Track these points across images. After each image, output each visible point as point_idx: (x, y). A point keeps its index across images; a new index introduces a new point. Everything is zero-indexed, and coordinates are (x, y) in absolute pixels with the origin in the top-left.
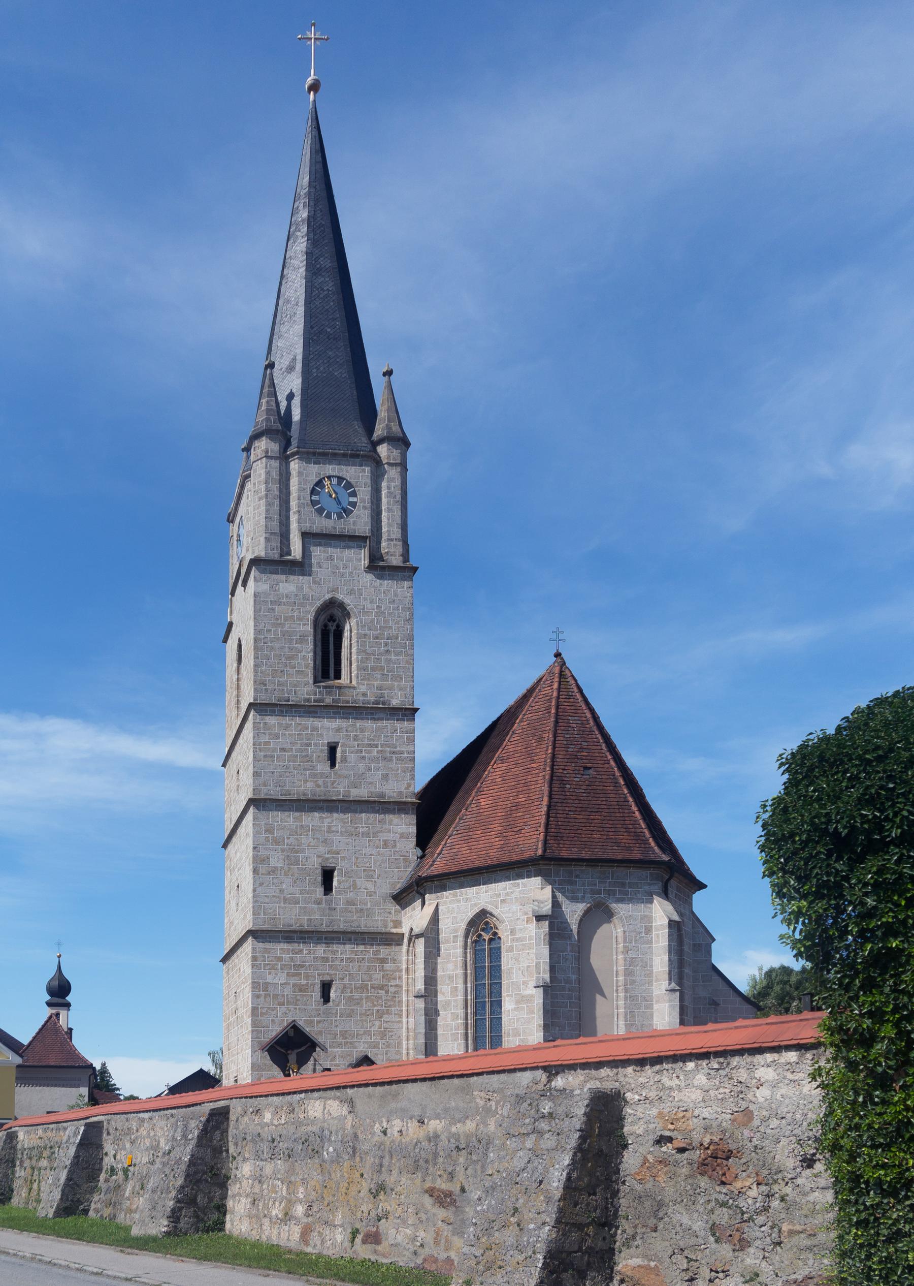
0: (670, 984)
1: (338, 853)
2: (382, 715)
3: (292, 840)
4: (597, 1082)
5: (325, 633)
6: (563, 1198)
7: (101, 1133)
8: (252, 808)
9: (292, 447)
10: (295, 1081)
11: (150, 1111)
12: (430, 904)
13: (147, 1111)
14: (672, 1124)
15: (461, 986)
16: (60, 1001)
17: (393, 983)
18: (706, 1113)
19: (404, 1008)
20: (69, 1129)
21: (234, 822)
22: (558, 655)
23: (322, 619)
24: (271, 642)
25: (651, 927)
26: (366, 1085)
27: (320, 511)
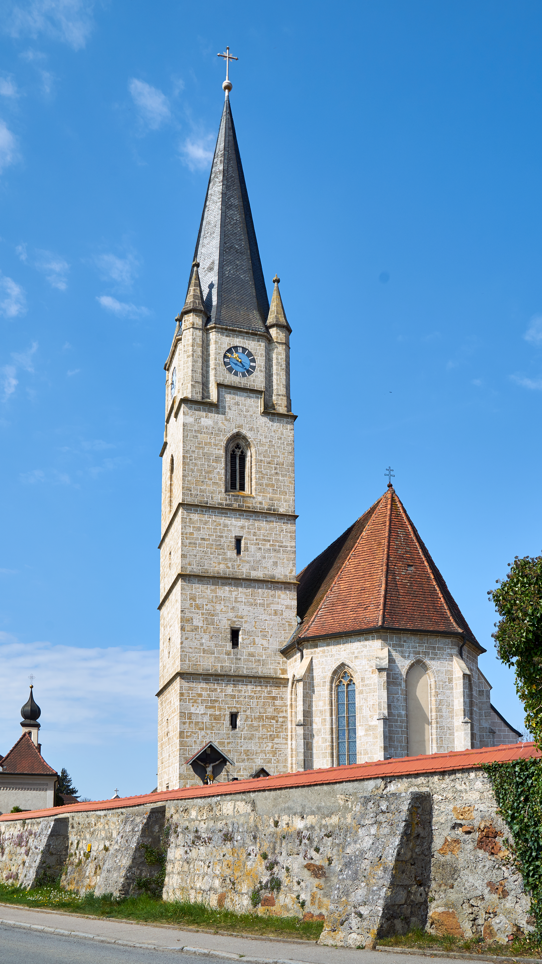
1: (242, 618)
2: (273, 519)
3: (209, 606)
4: (416, 787)
6: (395, 868)
7: (68, 827)
8: (180, 580)
9: (211, 323)
10: (213, 787)
11: (105, 810)
12: (307, 658)
13: (103, 810)
14: (462, 815)
15: (328, 718)
16: (32, 722)
17: (281, 715)
18: (482, 807)
19: (289, 734)
20: (42, 823)
21: (167, 591)
22: (390, 486)
23: (231, 446)
24: (195, 460)
25: (452, 678)
26: (264, 790)
27: (230, 370)
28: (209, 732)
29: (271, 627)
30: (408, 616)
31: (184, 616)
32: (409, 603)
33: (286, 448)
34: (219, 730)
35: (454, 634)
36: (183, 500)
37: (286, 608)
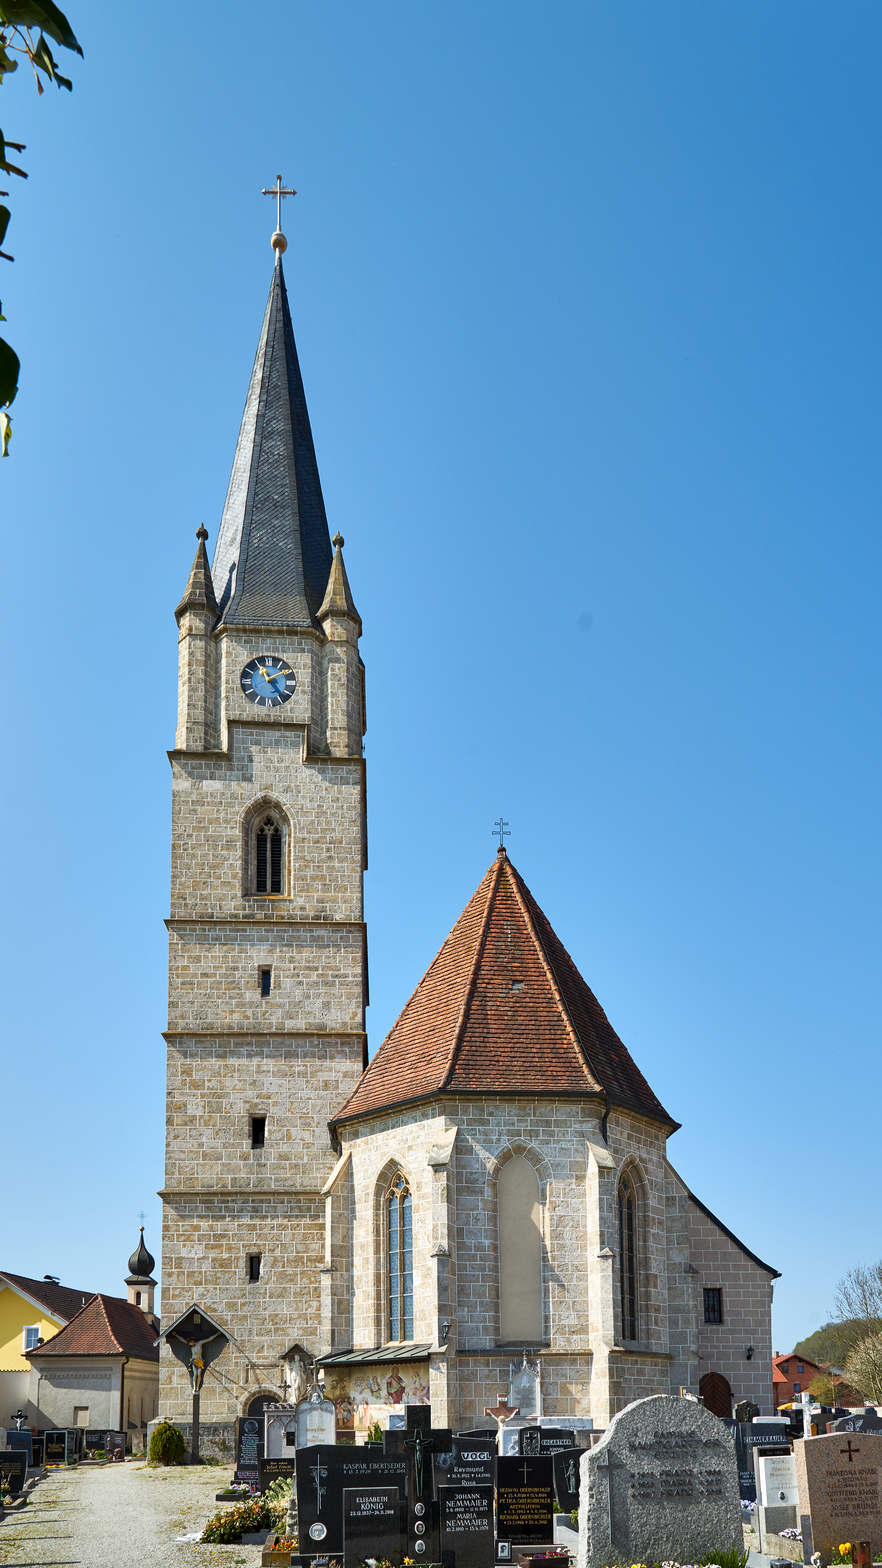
0: (601, 1249)
1: (269, 1098)
5: (261, 839)
16: (141, 1278)
23: (257, 822)
24: (193, 849)
27: (252, 697)
28: (210, 1287)
29: (317, 1109)
30: (500, 1068)
31: (172, 1102)
32: (506, 1045)
33: (346, 815)
34: (228, 1283)
35: (589, 1095)
36: (173, 916)
37: (344, 1077)
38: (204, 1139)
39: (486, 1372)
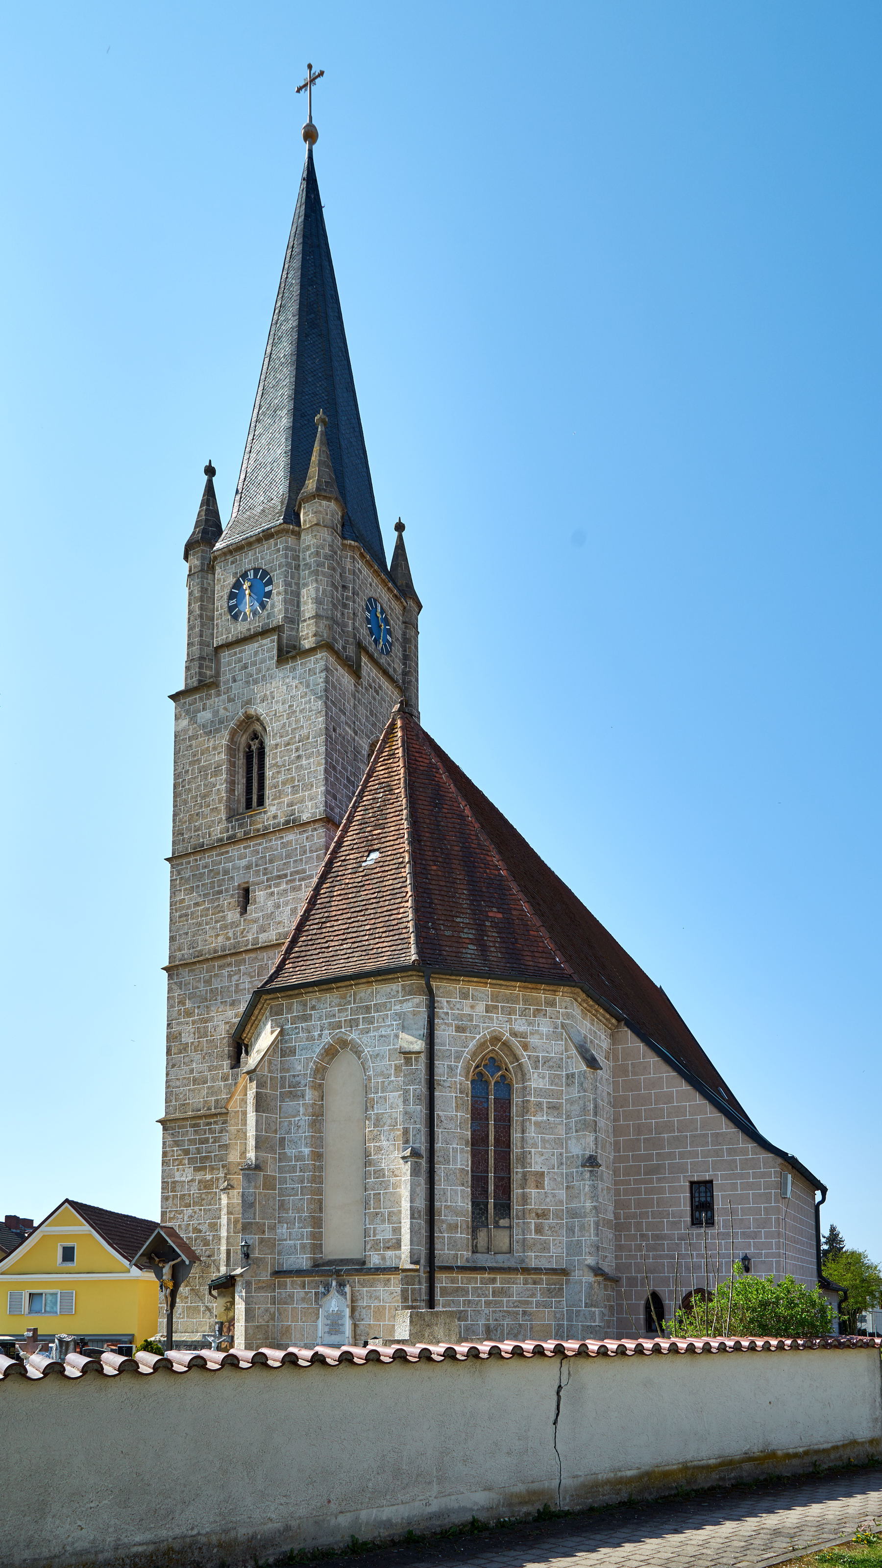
23: (243, 740)
34: (210, 1204)
38: (194, 1065)
39: (302, 1295)
